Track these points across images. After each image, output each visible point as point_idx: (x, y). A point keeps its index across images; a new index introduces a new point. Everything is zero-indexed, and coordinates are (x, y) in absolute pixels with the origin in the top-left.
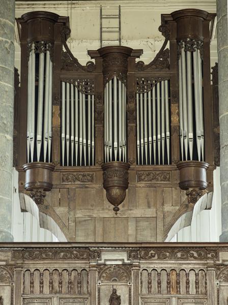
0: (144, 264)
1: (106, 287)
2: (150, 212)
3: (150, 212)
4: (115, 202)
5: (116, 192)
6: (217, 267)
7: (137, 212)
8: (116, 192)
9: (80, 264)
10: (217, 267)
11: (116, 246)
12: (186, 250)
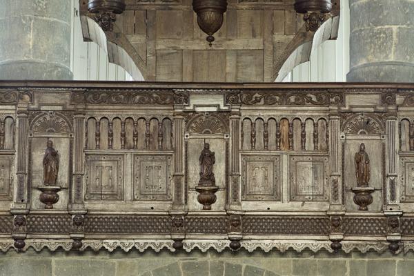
0: (246, 111)
1: (195, 141)
2: (255, 43)
3: (255, 43)
4: (209, 29)
5: (210, 15)
6: (343, 115)
7: (238, 43)
8: (210, 15)
9: (161, 111)
10: (343, 115)
11: (210, 88)
12: (302, 92)
